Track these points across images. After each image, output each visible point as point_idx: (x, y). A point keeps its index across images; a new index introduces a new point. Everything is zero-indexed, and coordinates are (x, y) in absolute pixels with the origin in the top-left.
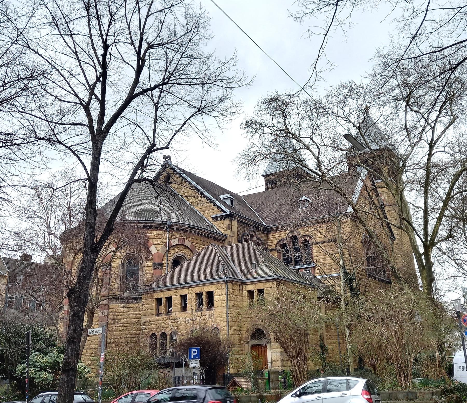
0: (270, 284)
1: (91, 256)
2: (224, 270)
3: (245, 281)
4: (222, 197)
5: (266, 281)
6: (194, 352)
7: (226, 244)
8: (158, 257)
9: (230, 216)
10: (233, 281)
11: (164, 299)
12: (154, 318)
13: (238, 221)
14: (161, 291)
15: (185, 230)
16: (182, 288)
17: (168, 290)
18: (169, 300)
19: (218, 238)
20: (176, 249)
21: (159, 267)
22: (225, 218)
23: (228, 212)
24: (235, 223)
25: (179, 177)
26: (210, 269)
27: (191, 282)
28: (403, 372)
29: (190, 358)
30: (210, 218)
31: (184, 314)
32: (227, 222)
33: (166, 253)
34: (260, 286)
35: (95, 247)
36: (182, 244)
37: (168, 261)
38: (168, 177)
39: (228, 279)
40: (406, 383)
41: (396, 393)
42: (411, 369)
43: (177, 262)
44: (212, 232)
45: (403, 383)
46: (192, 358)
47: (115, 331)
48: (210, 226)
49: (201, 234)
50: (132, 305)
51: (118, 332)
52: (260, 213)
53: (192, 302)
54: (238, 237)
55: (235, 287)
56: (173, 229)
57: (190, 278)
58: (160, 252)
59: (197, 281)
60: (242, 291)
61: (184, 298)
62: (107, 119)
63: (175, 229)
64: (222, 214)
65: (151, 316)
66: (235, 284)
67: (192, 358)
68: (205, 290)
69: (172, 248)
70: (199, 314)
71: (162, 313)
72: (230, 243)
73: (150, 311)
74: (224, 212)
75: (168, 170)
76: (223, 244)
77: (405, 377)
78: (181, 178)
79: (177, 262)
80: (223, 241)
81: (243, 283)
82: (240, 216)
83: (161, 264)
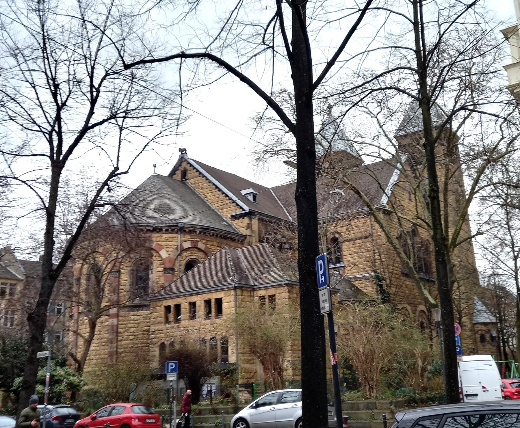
0: (280, 290)
1: (49, 283)
2: (233, 275)
3: (256, 287)
4: (243, 192)
5: (277, 286)
6: (172, 366)
7: (246, 244)
8: (170, 261)
9: (250, 214)
10: (242, 287)
11: (172, 306)
12: (162, 326)
13: (259, 219)
14: (169, 298)
15: (198, 232)
16: (191, 295)
17: (177, 297)
18: (178, 307)
19: (237, 238)
20: (188, 252)
21: (170, 272)
22: (245, 216)
23: (247, 209)
24: (255, 222)
25: (196, 172)
26: (220, 275)
27: (200, 288)
28: (368, 383)
29: (168, 372)
30: (229, 217)
31: (191, 322)
32: (246, 220)
33: (177, 257)
34: (271, 292)
35: (53, 274)
36: (195, 247)
37: (179, 266)
38: (184, 174)
39: (237, 285)
40: (370, 394)
41: (357, 403)
42: (376, 380)
43: (190, 265)
44: (228, 233)
45: (368, 393)
46: (170, 371)
47: (125, 340)
48: (228, 225)
49: (217, 236)
50: (139, 313)
51: (129, 341)
52: (287, 208)
53: (201, 310)
54: (260, 237)
55: (245, 293)
56: (185, 231)
57: (200, 284)
58: (171, 256)
59: (206, 287)
60: (253, 297)
61: (193, 305)
62: (65, 148)
63: (187, 231)
64: (240, 212)
65: (160, 324)
66: (245, 290)
67: (170, 371)
68: (213, 296)
69: (184, 252)
70: (208, 322)
71: (170, 322)
72: (250, 244)
73: (159, 319)
74: (244, 210)
75: (184, 164)
76: (243, 244)
77: (370, 388)
78: (198, 173)
79: (190, 265)
80: (242, 241)
81: (253, 289)
82: (261, 214)
83: (172, 269)
